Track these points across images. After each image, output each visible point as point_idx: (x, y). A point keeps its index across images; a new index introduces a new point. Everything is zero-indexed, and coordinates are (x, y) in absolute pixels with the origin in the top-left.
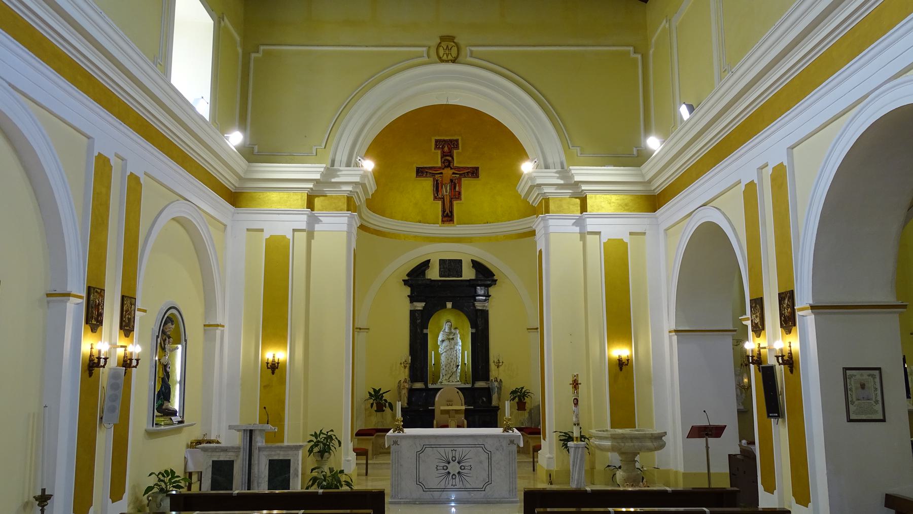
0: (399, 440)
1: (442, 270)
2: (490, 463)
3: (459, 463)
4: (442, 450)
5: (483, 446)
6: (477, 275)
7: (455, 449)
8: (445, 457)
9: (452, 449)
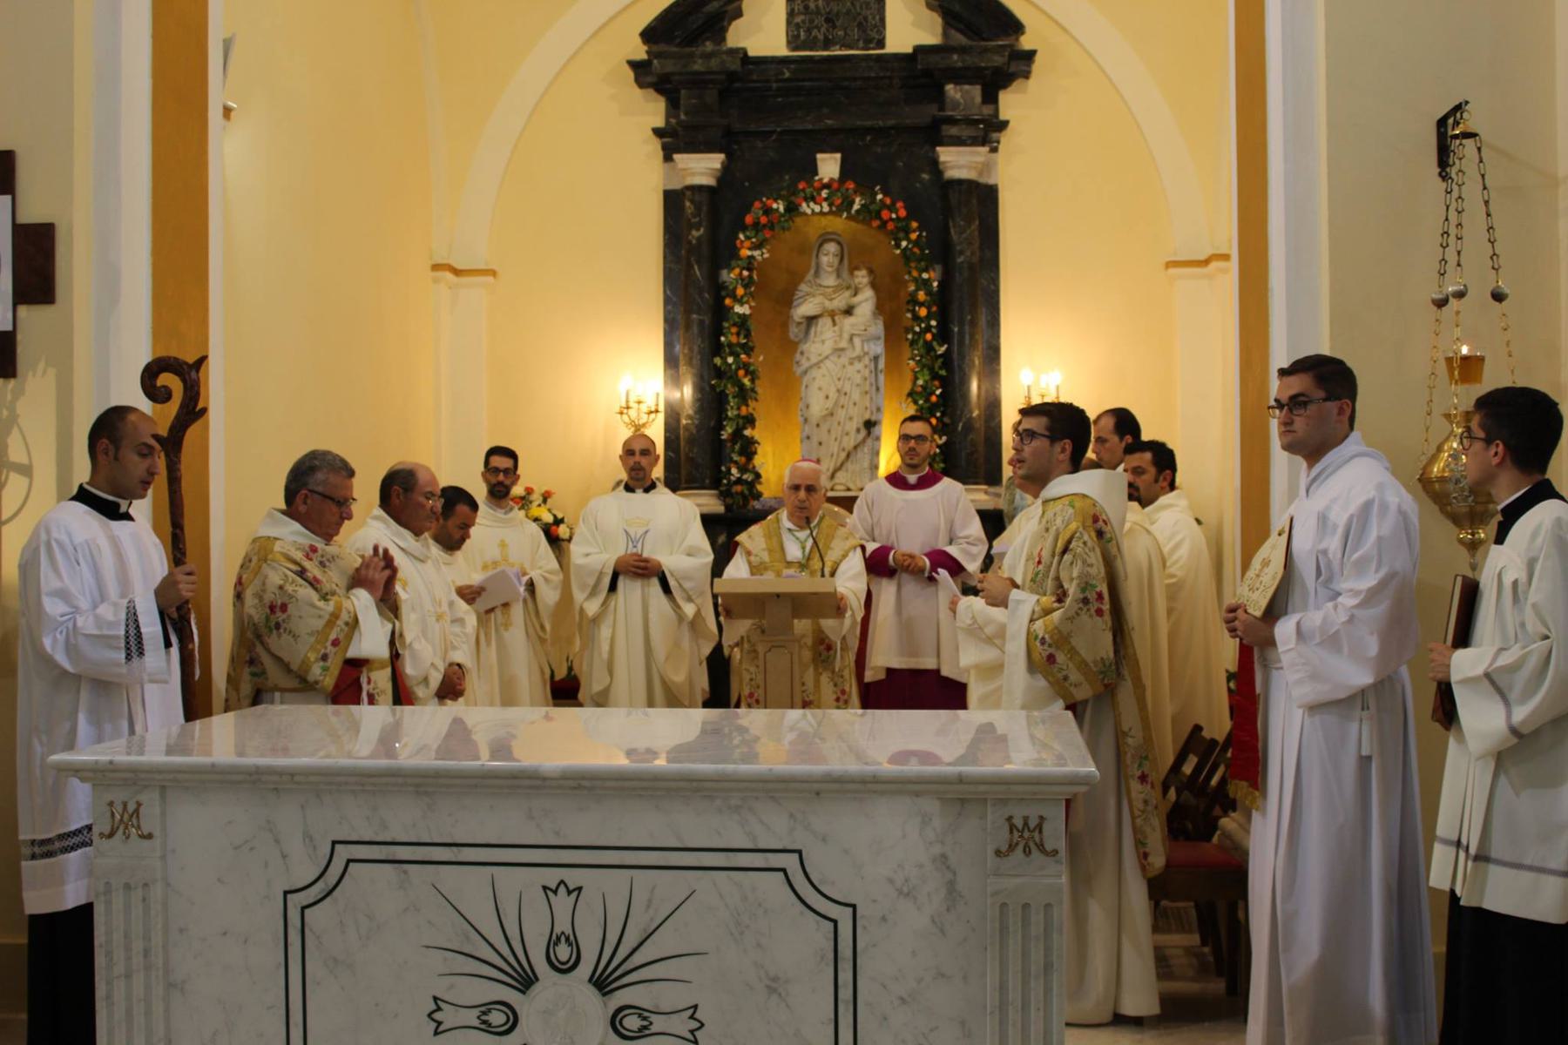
0: (151, 803)
1: (798, 19)
2: (846, 994)
3: (602, 983)
4: (470, 887)
5: (790, 862)
6: (945, 34)
7: (574, 877)
8: (506, 951)
9: (551, 877)
